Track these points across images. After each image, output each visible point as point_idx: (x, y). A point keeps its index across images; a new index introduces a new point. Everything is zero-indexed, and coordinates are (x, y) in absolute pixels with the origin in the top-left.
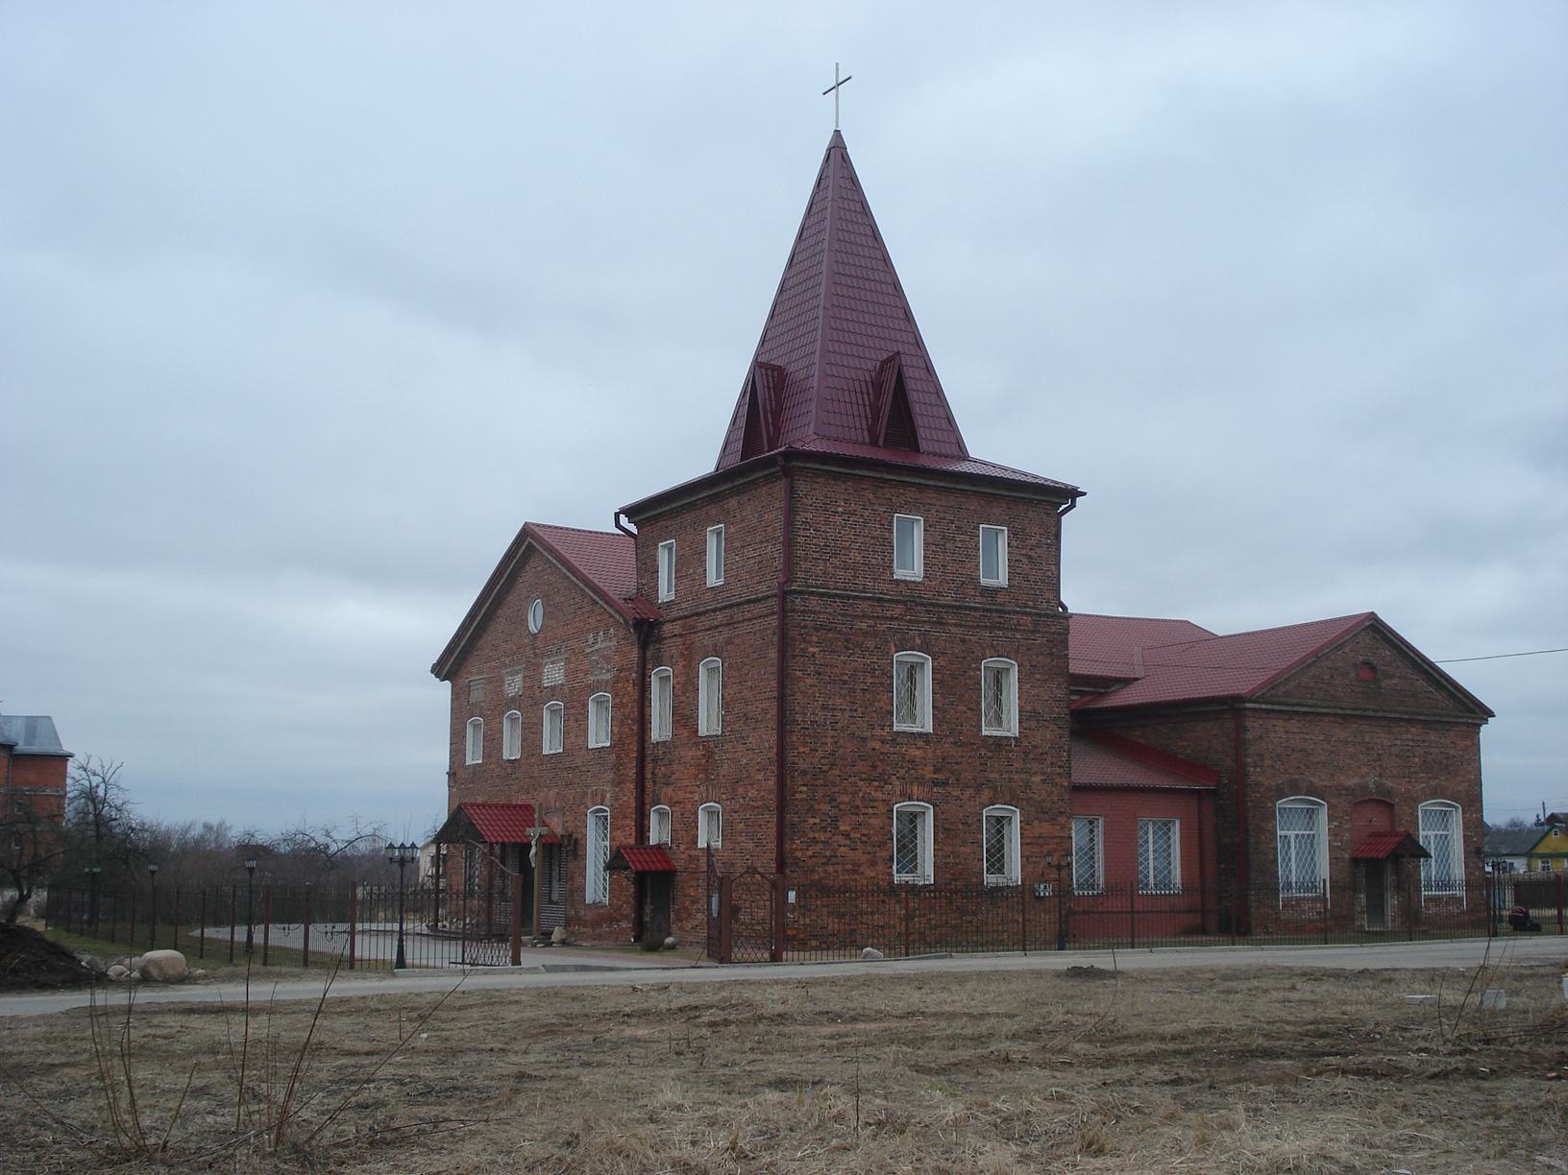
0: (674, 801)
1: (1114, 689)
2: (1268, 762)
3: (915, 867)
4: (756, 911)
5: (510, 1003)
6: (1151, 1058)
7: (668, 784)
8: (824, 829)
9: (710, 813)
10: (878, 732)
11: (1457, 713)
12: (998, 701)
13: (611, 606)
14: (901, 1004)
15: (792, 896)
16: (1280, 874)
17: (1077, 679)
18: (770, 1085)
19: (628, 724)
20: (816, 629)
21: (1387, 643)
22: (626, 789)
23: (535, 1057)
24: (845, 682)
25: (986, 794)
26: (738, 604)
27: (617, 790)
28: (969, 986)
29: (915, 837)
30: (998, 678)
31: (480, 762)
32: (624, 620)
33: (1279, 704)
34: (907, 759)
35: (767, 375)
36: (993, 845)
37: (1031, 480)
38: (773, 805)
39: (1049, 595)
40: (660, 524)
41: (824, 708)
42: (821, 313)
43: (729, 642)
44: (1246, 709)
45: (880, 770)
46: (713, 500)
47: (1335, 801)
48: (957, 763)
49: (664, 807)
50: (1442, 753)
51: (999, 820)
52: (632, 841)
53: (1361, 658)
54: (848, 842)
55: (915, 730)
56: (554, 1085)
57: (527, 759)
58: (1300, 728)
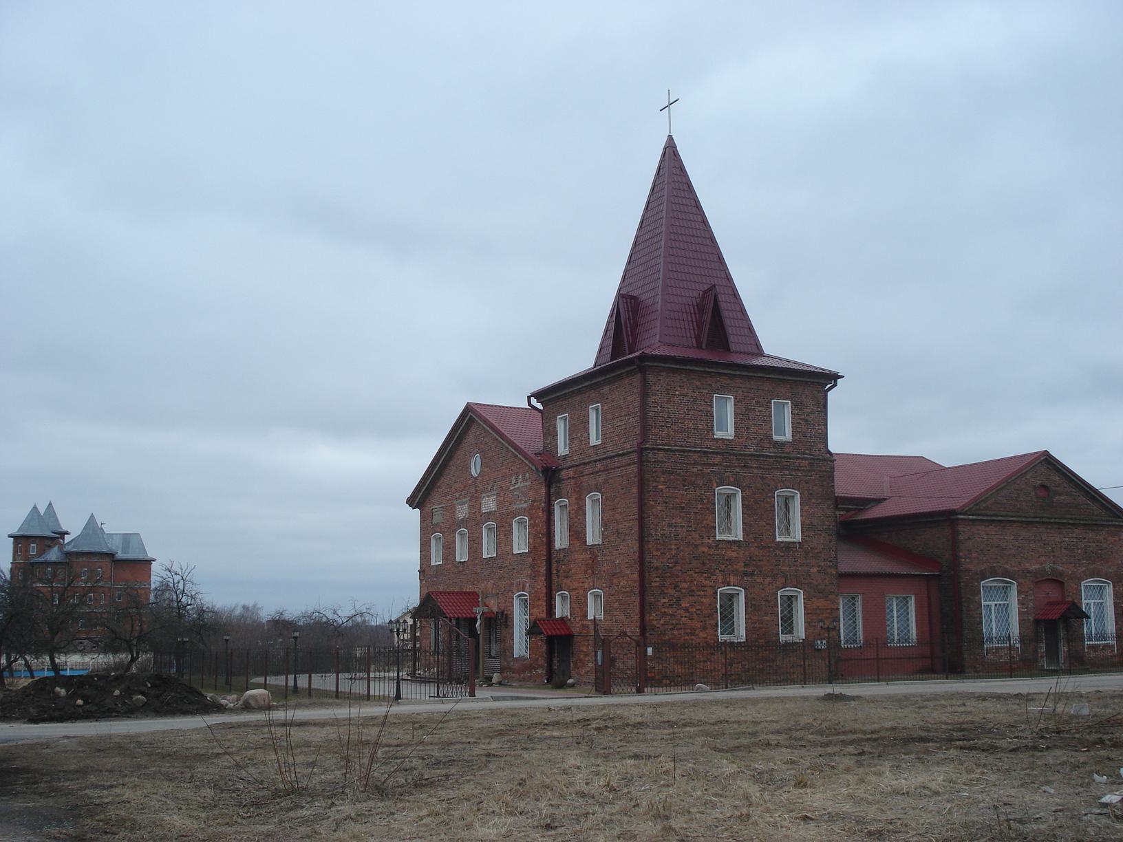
0: (571, 588)
1: (869, 506)
2: (975, 555)
3: (733, 630)
4: (626, 661)
5: (474, 718)
6: (852, 742)
7: (567, 577)
9: (596, 596)
10: (706, 541)
12: (787, 518)
13: (526, 458)
14: (714, 716)
15: (650, 651)
16: (984, 630)
17: (839, 502)
18: (630, 757)
20: (663, 473)
21: (1057, 471)
23: (495, 745)
24: (683, 508)
25: (780, 581)
26: (611, 457)
28: (760, 706)
29: (733, 610)
30: (786, 502)
31: (441, 563)
33: (979, 515)
34: (726, 558)
36: (785, 616)
37: (806, 369)
38: (637, 590)
41: (670, 525)
42: (662, 260)
43: (606, 482)
44: (958, 519)
46: (591, 387)
47: (1022, 581)
50: (1097, 546)
51: (790, 598)
52: (544, 615)
53: (1039, 482)
54: (687, 614)
55: (731, 539)
56: (508, 758)
58: (996, 531)
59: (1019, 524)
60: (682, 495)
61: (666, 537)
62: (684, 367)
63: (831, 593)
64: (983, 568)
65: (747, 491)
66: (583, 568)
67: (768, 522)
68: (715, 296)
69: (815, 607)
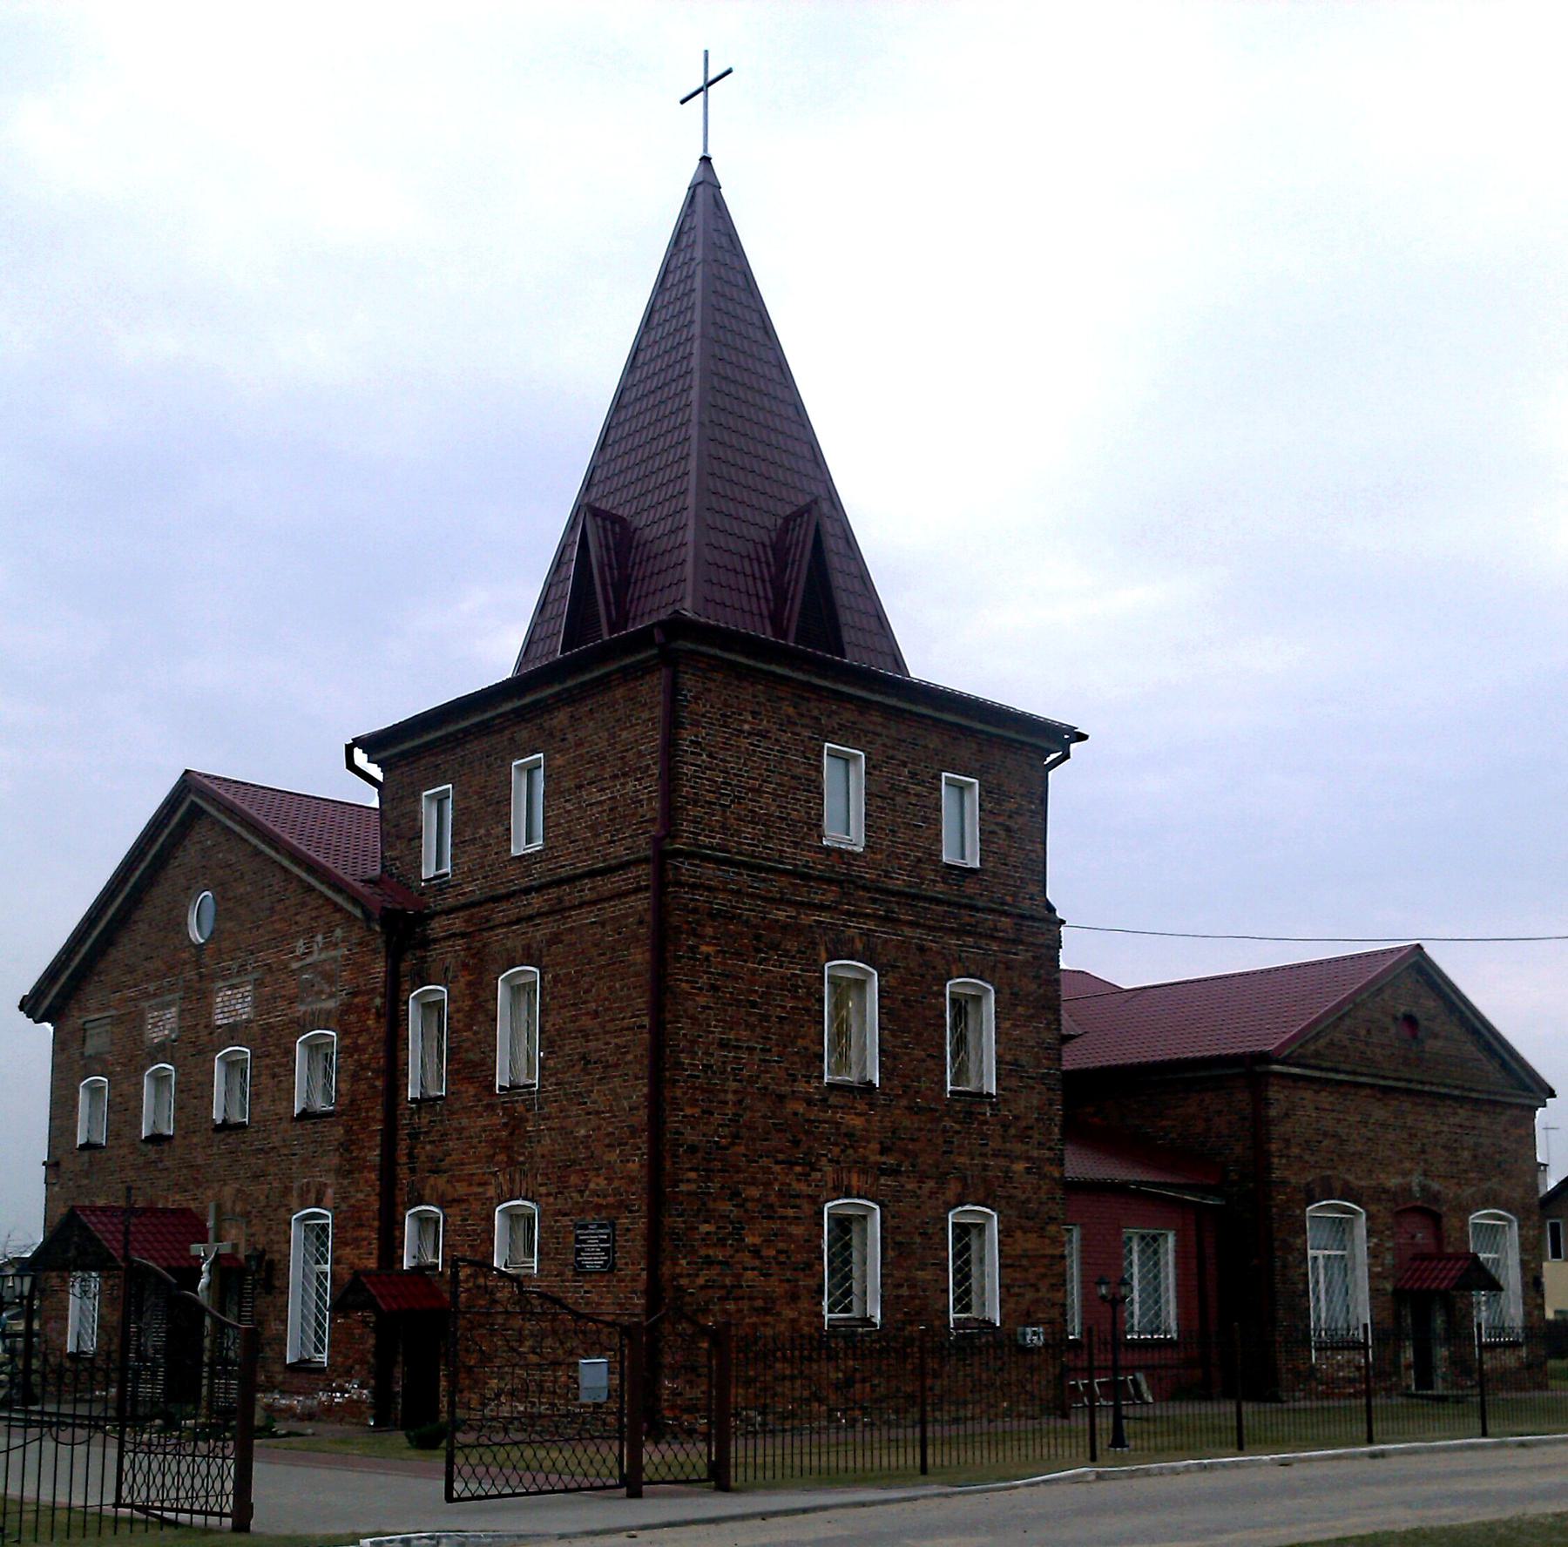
0: (449, 1198)
2: (1296, 1151)
7: (436, 1171)
8: (722, 1242)
11: (1509, 1091)
19: (367, 1079)
22: (362, 1182)
24: (754, 1005)
25: (953, 1189)
27: (346, 1182)
32: (364, 912)
35: (605, 530)
39: (1033, 889)
40: (424, 762)
41: (723, 1045)
43: (555, 939)
45: (804, 1147)
46: (520, 715)
47: (1373, 1208)
48: (912, 1140)
49: (432, 1208)
50: (1493, 1144)
51: (962, 1230)
52: (372, 1264)
53: (1403, 1009)
54: (757, 1263)
57: (184, 1138)
59: (1368, 1091)
60: (753, 972)
61: (714, 1073)
62: (765, 667)
63: (1052, 1219)
64: (1310, 1179)
65: (890, 977)
66: (484, 1149)
67: (931, 1051)
68: (817, 531)
69: (1019, 1252)
